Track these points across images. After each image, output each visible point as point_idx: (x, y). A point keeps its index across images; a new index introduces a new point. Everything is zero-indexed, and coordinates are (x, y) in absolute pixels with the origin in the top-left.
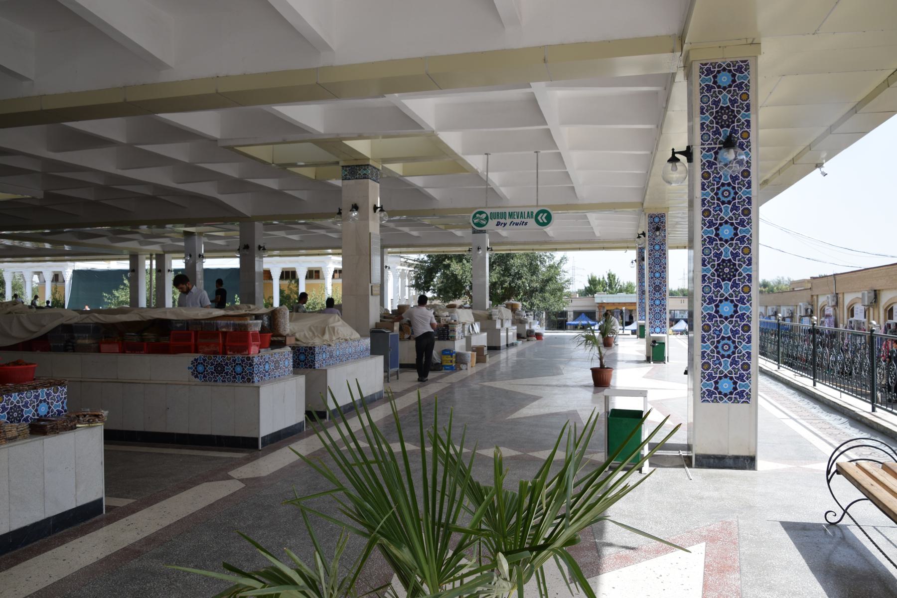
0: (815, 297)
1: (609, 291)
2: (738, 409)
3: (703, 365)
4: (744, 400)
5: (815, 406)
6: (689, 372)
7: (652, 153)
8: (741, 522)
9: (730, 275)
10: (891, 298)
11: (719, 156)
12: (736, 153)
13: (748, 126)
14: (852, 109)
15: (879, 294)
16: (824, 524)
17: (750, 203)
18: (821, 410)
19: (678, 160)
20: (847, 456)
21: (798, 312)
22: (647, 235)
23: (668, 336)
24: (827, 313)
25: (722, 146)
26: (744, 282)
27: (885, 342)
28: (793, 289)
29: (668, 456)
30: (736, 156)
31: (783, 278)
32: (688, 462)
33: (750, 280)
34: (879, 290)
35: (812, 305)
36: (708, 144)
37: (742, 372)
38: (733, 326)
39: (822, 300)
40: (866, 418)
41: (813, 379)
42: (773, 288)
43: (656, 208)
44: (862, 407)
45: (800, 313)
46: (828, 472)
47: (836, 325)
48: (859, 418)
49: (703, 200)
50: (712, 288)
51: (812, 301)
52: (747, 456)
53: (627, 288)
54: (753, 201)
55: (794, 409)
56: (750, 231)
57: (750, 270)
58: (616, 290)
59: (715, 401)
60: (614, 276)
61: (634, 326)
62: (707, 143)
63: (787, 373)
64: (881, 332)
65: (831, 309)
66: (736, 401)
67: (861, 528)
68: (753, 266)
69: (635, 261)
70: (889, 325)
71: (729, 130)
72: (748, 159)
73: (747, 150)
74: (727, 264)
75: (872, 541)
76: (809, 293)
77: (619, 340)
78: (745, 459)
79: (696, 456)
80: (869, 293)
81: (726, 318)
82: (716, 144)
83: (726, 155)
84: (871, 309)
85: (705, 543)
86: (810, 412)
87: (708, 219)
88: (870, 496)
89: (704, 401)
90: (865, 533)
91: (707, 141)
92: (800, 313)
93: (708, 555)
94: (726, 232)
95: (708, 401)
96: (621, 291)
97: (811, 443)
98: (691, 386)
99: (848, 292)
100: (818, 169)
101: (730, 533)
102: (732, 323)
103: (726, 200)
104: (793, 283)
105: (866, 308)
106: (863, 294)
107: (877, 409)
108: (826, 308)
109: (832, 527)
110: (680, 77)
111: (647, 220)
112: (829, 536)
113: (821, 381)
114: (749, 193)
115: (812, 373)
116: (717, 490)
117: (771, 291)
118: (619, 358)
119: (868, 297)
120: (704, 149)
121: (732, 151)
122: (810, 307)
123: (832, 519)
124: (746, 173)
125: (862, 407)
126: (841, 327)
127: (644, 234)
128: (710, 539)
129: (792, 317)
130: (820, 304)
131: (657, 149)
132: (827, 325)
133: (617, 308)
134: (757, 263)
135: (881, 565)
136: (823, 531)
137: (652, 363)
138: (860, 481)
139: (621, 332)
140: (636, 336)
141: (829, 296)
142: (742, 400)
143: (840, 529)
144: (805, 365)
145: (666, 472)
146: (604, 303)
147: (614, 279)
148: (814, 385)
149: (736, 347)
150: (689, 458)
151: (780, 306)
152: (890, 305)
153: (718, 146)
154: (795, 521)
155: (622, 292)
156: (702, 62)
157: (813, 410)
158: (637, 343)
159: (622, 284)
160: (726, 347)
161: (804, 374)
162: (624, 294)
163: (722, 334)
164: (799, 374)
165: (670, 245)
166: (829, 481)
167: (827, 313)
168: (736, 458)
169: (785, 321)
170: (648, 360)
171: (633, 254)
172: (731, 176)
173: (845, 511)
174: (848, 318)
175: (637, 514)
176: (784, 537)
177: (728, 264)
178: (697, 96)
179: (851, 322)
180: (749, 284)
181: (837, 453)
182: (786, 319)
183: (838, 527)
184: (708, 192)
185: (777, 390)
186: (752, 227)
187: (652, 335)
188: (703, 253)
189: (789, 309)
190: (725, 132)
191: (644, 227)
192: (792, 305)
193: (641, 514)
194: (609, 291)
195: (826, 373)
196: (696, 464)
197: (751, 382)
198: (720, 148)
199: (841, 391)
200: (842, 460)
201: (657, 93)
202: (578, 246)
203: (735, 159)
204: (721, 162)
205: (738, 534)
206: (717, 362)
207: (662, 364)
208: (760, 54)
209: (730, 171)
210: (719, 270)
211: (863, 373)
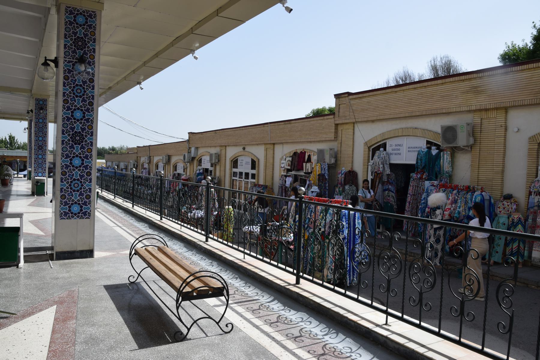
0: (139, 158)
1: (10, 148)
2: (85, 221)
3: (61, 196)
4: (87, 217)
5: (132, 218)
6: (53, 201)
7: (37, 57)
8: (80, 289)
9: (80, 141)
10: (176, 160)
11: (75, 67)
12: (86, 67)
13: (94, 52)
14: (155, 54)
15: (171, 157)
16: (128, 283)
17: (93, 99)
18: (135, 221)
19: (49, 65)
20: (143, 243)
21: (130, 166)
22: (34, 112)
23: (47, 179)
24: (145, 167)
25: (77, 61)
26: (88, 146)
27: (172, 183)
28: (128, 152)
29: (38, 255)
30: (86, 69)
31: (124, 146)
32: (51, 258)
33: (92, 145)
34: (171, 156)
35: (137, 162)
36: (68, 58)
37: (86, 200)
38: (81, 172)
39: (143, 159)
40: (157, 224)
41: (132, 204)
42: (118, 151)
43: (41, 95)
44: (155, 217)
45: (131, 166)
46: (130, 254)
47: (149, 174)
48: (154, 224)
49: (64, 93)
50: (68, 149)
51: (138, 160)
52: (88, 250)
53: (23, 146)
54: (95, 98)
55: (117, 219)
56: (63, 113)
57: (92, 139)
58: (15, 147)
59: (69, 218)
60: (14, 138)
61: (25, 172)
62: (68, 57)
63: (119, 201)
64: (171, 178)
65: (147, 165)
66: (82, 218)
67: (146, 283)
68: (94, 137)
69: (27, 128)
70: (175, 174)
71: (82, 52)
72: (93, 72)
73: (93, 66)
74: (78, 134)
75: (151, 288)
76: (135, 155)
77: (14, 181)
78: (86, 252)
79: (56, 253)
80: (166, 157)
81: (77, 168)
82: (74, 59)
83: (79, 67)
84: (167, 165)
85: (56, 306)
86: (129, 222)
87: (67, 105)
88: (150, 265)
89: (62, 218)
90: (148, 285)
91: (68, 56)
92: (131, 166)
93: (57, 313)
94: (78, 114)
95: (64, 218)
96: (18, 148)
97: (127, 239)
98: (54, 211)
99: (155, 156)
100: (138, 85)
101: (73, 297)
102: (80, 171)
103: (79, 95)
104: (128, 149)
105: (164, 164)
106: (163, 157)
107: (163, 219)
108: (145, 164)
109: (132, 284)
110: (53, 11)
111: (34, 102)
112: (130, 289)
113: (136, 204)
114: (93, 92)
115: (132, 200)
116: (68, 272)
117: (117, 153)
118: (13, 193)
119: (166, 159)
120: (66, 61)
121: (83, 65)
122: (136, 163)
123: (132, 280)
124: (92, 80)
125: (155, 217)
126: (152, 175)
127: (32, 111)
128: (60, 302)
129: (126, 168)
130: (141, 162)
131: (39, 56)
132: (144, 174)
133: (15, 160)
134: (96, 135)
135: (154, 300)
136: (127, 288)
137: (35, 196)
138: (145, 258)
139: (16, 176)
140: (26, 179)
141: (146, 157)
142: (86, 217)
143: (136, 285)
144: (129, 196)
145: (36, 265)
146: (5, 155)
147: (14, 140)
148: (133, 207)
149: (82, 185)
150: (52, 254)
151: (120, 162)
152: (176, 163)
153: (75, 60)
154: (112, 284)
155: (19, 149)
156: (67, 5)
157: (131, 221)
158: (28, 183)
159: (20, 144)
160: (76, 185)
161: (128, 201)
162: (20, 150)
163: (74, 177)
164: (125, 201)
165: (49, 120)
166: (130, 259)
167: (145, 167)
168: (82, 252)
169: (122, 171)
170: (33, 194)
171: (25, 124)
172: (82, 80)
173: (139, 275)
174: (155, 170)
175: (12, 295)
176: (105, 294)
177: (79, 135)
178: (63, 27)
179: (157, 172)
180: (91, 148)
181: (137, 241)
182: (123, 170)
183: (135, 284)
184: (67, 89)
185: (113, 210)
186: (94, 113)
187: (36, 178)
188: (63, 126)
189: (125, 164)
190: (79, 52)
191: (32, 107)
192: (126, 162)
193: (15, 294)
194: (10, 148)
195: (139, 200)
196: (56, 258)
197: (91, 206)
198: (76, 62)
199: (146, 210)
200: (139, 245)
201: (41, 18)
202: (20, 117)
203: (85, 71)
204: (76, 70)
205: (78, 297)
206: (71, 194)
207: (43, 197)
208: (103, 10)
209: (82, 78)
210: (73, 138)
211: (157, 199)
